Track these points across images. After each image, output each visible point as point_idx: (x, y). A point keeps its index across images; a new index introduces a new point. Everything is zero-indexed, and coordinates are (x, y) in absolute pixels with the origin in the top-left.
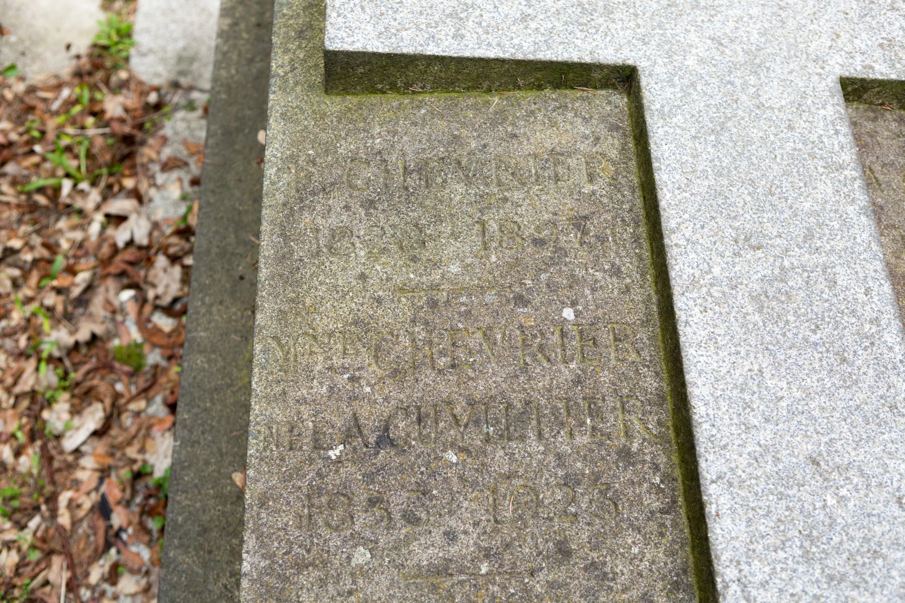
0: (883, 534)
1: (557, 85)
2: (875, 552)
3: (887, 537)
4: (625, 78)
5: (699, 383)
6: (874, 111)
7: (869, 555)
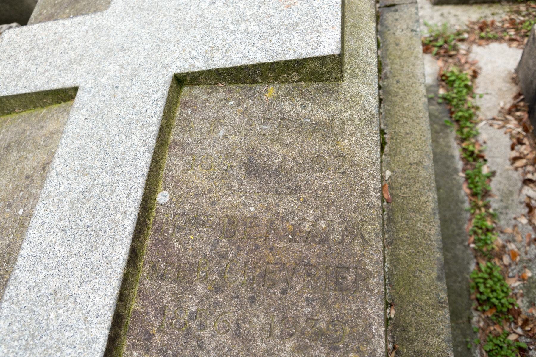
0: (68, 338)
1: (25, 107)
2: (59, 348)
3: (69, 340)
4: (180, 81)
5: (26, 248)
6: (212, 88)
7: (55, 349)
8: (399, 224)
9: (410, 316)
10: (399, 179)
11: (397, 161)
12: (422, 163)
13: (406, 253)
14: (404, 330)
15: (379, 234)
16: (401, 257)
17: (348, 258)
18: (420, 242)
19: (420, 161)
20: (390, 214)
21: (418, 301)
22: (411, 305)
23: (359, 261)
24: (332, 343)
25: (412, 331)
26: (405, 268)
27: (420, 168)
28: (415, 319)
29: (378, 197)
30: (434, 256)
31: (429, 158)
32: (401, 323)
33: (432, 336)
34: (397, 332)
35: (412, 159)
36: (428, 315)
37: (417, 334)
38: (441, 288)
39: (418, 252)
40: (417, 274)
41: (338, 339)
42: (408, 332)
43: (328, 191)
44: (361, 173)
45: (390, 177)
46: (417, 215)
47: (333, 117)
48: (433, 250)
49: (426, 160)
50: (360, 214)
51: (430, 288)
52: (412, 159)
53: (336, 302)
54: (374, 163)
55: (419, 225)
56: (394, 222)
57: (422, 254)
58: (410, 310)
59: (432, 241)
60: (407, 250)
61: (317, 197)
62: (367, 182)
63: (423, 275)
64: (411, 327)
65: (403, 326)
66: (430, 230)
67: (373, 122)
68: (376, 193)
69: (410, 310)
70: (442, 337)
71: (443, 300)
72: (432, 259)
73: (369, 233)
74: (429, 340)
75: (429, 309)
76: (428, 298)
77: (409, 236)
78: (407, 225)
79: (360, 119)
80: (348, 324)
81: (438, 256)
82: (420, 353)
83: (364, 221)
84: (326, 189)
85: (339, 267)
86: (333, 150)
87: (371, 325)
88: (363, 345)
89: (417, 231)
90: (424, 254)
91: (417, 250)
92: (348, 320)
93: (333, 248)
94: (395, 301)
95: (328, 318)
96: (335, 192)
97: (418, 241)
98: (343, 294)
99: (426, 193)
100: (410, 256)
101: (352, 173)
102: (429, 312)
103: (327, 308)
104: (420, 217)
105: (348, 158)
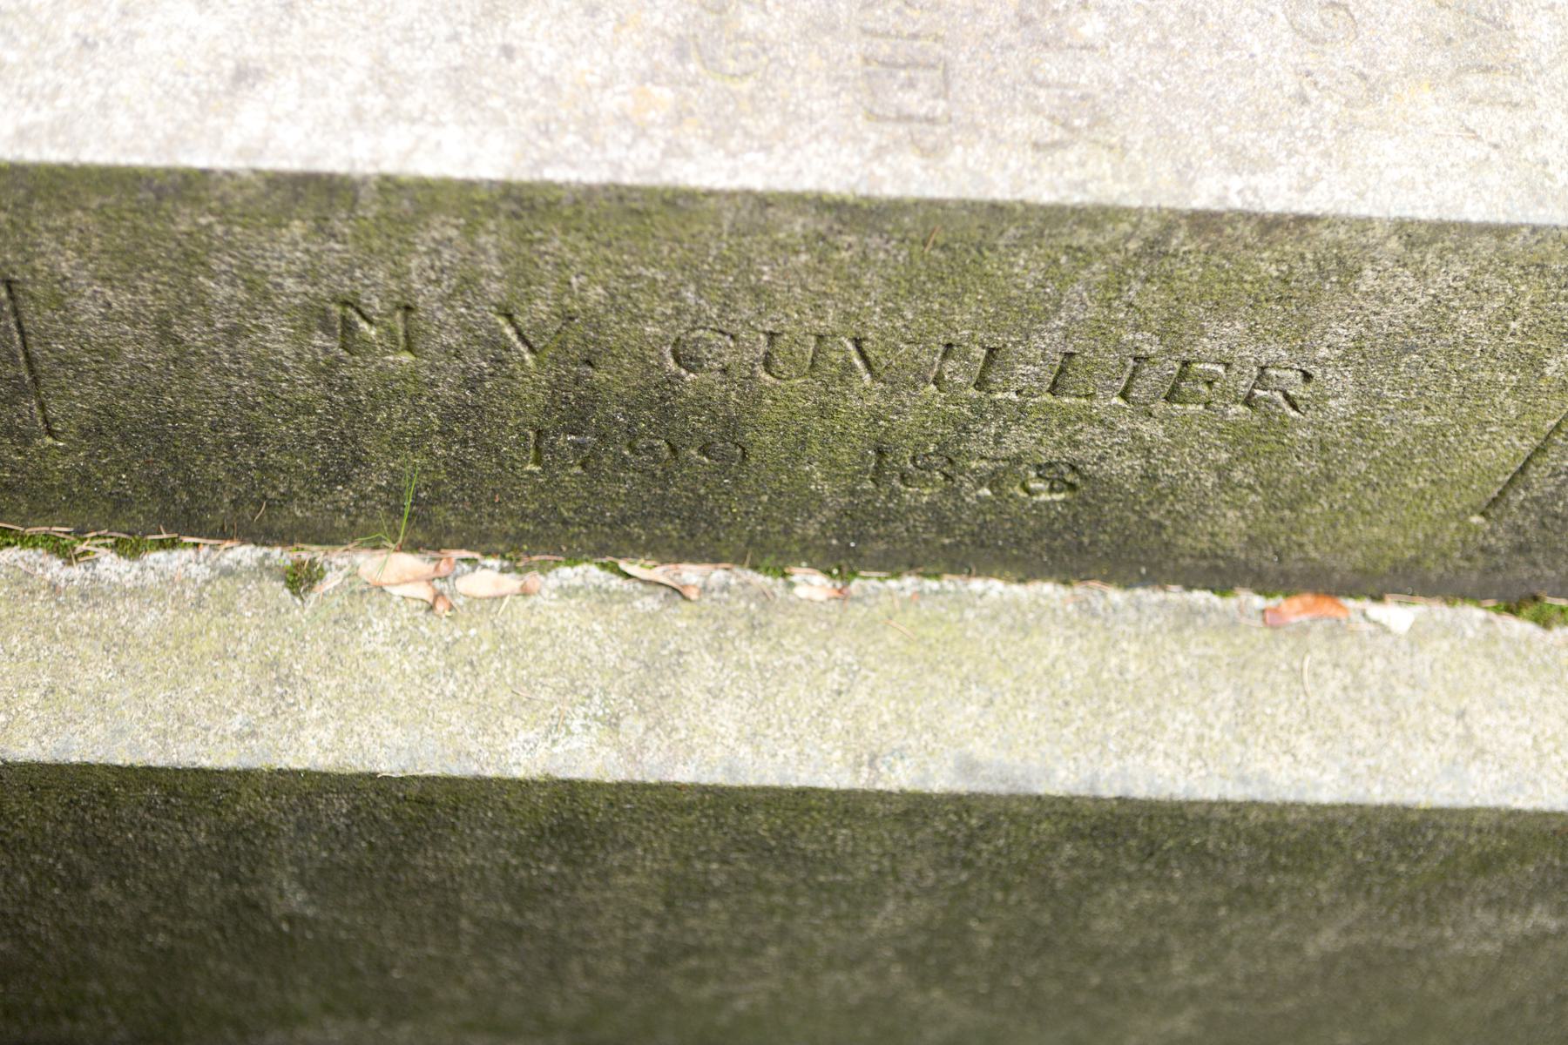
8: (1176, 647)
9: (806, 649)
10: (1379, 663)
11: (1466, 665)
12: (1474, 757)
13: (1057, 659)
14: (753, 627)
15: (1085, 191)
16: (1036, 639)
17: (981, 96)
18: (1109, 714)
19: (1482, 751)
20: (1213, 616)
21: (870, 682)
22: (849, 659)
23: (975, 128)
24: (697, 45)
25: (754, 653)
26: (994, 652)
27: (1449, 749)
28: (799, 667)
29: (1226, 198)
30: (1058, 759)
31: (1505, 791)
32: (779, 620)
33: (743, 718)
34: (743, 604)
35: (1487, 720)
36: (821, 712)
37: (739, 665)
38: (932, 767)
39: (1067, 704)
40: (974, 690)
41: (712, 60)
42: (749, 639)
43: (1219, 46)
44: (1312, 150)
45: (1385, 630)
46: (1226, 716)
47: (1538, 73)
48: (1081, 755)
49: (1492, 777)
50: (1149, 140)
51: (926, 728)
52: (1487, 720)
53: (827, 58)
54: (1361, 196)
55: (1181, 716)
56: (1179, 629)
57: (1058, 714)
58: (830, 653)
59: (1120, 757)
60: (1069, 664)
61: (1193, 15)
62: (1280, 170)
63: (973, 709)
64: (770, 652)
65: (769, 623)
66: (1167, 755)
67: (1540, 203)
68: (1240, 192)
69: (830, 653)
70: (744, 751)
71: (883, 769)
72: (1046, 747)
73: (1082, 164)
74: (725, 705)
75: (844, 717)
76: (886, 718)
77: (1129, 676)
78: (1176, 674)
79: (1546, 164)
80: (762, 89)
81: (1062, 774)
82: (679, 671)
83: (1125, 151)
84: (1224, 43)
85: (945, 72)
86: (1391, 68)
87: (767, 149)
88: (702, 127)
89: (1156, 706)
90: (1065, 724)
91: (1073, 702)
92: (774, 90)
93: (1012, 55)
94: (858, 605)
95: (773, 35)
96: (1220, 67)
97: (1112, 705)
98: (856, 79)
99: (1335, 759)
100: (1047, 672)
101: (1307, 124)
102: (830, 717)
103: (804, 34)
104: (1218, 725)
105: (1365, 114)
